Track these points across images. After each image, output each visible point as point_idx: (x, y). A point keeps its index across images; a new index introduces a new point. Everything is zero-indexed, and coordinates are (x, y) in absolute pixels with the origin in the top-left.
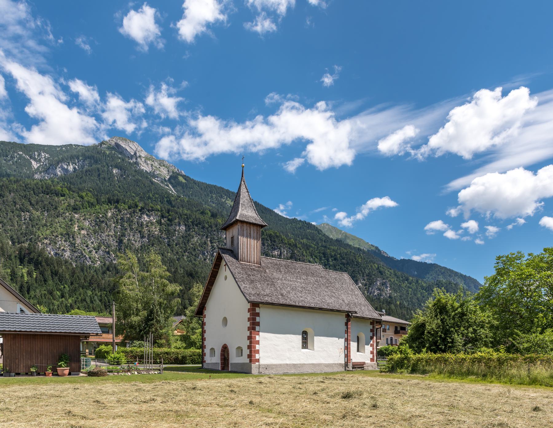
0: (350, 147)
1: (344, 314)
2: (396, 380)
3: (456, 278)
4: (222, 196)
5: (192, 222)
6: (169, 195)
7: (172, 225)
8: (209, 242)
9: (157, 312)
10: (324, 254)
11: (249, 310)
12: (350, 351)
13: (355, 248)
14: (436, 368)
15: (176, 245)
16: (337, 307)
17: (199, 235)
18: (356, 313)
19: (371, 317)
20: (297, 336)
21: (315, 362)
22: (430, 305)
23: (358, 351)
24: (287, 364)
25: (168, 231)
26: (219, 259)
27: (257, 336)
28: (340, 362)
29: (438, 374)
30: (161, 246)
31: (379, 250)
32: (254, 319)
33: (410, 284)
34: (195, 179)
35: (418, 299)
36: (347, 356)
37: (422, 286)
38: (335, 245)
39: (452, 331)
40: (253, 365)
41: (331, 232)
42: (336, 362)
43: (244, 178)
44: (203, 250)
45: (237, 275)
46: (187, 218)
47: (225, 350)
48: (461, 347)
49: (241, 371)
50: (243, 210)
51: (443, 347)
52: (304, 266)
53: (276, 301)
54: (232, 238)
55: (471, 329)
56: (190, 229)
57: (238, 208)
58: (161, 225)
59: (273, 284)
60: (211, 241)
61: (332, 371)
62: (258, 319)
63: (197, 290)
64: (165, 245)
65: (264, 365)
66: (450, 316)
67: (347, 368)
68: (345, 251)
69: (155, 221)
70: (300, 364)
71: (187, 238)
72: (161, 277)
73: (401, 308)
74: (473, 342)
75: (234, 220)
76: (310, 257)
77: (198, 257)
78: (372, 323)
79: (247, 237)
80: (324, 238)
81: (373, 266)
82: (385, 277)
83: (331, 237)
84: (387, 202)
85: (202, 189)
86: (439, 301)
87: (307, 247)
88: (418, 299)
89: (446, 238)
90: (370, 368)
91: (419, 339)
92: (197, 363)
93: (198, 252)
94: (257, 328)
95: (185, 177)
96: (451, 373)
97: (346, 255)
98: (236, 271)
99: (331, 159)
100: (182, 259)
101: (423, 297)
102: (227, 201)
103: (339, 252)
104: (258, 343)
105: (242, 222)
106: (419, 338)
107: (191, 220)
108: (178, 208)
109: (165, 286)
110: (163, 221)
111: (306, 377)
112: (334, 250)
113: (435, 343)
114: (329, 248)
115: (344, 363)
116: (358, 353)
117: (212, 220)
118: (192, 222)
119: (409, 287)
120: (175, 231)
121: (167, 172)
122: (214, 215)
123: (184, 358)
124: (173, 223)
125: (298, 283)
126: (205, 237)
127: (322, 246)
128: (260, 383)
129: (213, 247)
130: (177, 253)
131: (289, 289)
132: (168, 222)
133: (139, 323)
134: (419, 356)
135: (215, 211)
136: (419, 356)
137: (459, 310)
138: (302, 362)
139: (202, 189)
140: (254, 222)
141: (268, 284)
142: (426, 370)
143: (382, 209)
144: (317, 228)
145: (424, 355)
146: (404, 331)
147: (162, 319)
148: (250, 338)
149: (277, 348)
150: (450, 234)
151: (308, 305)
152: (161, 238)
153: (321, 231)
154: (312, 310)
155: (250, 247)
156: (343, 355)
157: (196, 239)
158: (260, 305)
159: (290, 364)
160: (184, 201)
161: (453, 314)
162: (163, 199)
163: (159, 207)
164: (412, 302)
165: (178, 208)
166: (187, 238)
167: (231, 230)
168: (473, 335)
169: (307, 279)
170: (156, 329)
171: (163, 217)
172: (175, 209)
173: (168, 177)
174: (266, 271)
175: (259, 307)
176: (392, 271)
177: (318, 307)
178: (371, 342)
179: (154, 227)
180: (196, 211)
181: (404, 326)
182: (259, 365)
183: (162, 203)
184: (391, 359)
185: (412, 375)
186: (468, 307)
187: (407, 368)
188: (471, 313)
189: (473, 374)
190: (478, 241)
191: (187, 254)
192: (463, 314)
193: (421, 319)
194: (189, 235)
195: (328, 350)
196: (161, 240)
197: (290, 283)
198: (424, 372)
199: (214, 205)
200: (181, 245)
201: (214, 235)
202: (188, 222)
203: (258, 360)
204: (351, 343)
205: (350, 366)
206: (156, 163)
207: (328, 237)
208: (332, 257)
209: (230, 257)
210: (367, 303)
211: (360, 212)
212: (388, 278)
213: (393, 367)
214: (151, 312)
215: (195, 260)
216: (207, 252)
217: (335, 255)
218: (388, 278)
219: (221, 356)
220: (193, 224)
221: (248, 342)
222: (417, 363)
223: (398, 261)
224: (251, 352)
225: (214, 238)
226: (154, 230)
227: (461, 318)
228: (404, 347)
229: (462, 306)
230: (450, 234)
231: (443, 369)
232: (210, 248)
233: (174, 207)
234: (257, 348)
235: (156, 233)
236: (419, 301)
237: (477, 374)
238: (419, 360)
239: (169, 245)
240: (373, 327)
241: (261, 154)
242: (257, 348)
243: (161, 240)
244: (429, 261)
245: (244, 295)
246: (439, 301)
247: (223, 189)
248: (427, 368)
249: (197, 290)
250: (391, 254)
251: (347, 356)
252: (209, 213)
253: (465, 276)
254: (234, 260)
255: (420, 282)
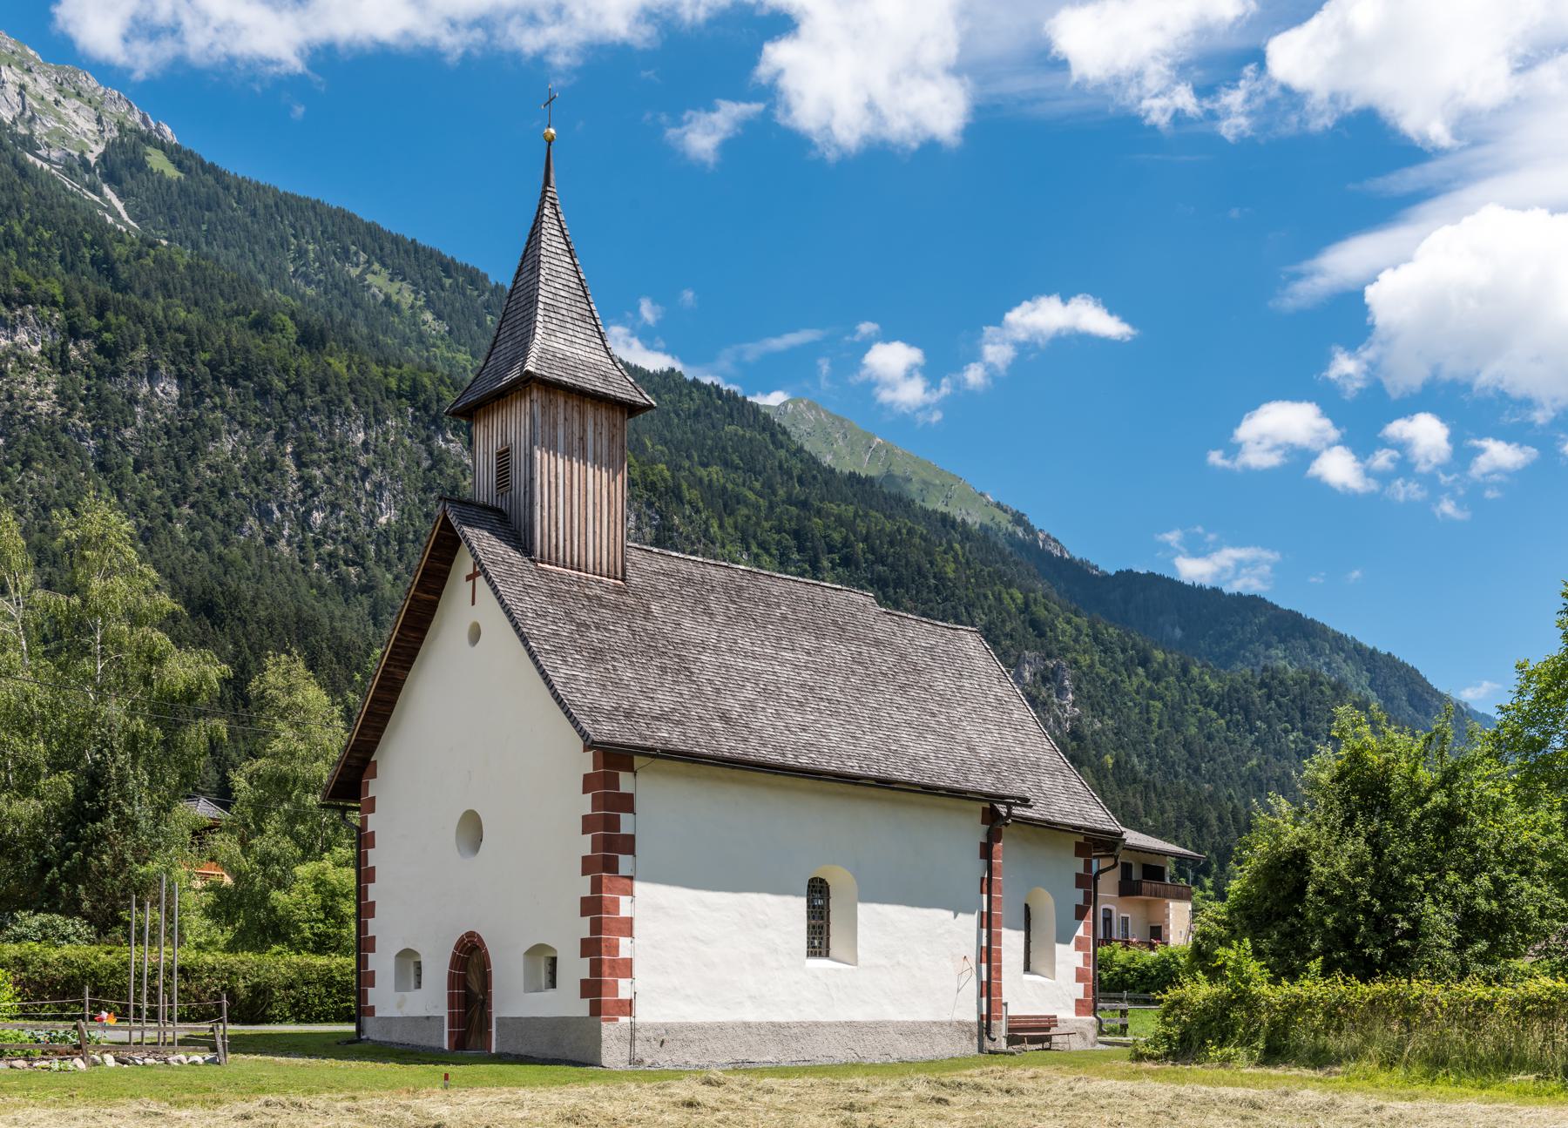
0: (956, 70)
1: (978, 807)
2: (1240, 1093)
3: (1339, 658)
4: (346, 251)
5: (213, 366)
6: (102, 235)
7: (116, 373)
8: (289, 462)
9: (122, 781)
10: (797, 534)
11: (588, 783)
12: (999, 970)
13: (928, 515)
14: (1368, 1040)
15: (137, 470)
16: (948, 777)
17: (243, 425)
18: (1025, 802)
19: (1079, 822)
20: (790, 899)
21: (859, 1015)
22: (1324, 777)
23: (1027, 969)
24: (747, 1025)
25: (101, 399)
26: (446, 546)
27: (624, 901)
28: (960, 1016)
29: (1381, 1064)
30: (64, 468)
31: (1029, 529)
32: (613, 824)
33: (1157, 680)
34: (222, 164)
35: (1187, 745)
36: (989, 989)
37: (1204, 692)
38: (845, 500)
39: (1412, 887)
40: (607, 1029)
41: (828, 440)
42: (946, 1018)
43: (553, 191)
44: (264, 495)
45: (530, 625)
46: (188, 344)
47: (470, 958)
48: (1446, 954)
49: (551, 1054)
50: (550, 333)
51: (1380, 952)
52: (801, 590)
53: (703, 746)
54: (504, 455)
55: (1483, 881)
56: (201, 397)
57: (530, 321)
58: (64, 372)
59: (684, 669)
60: (297, 456)
61: (928, 1056)
62: (626, 824)
63: (281, 682)
64: (84, 468)
65: (654, 1027)
66: (1402, 826)
67: (988, 1044)
68: (888, 526)
69: (36, 349)
70: (800, 1024)
71: (186, 436)
72: (136, 619)
73: (1120, 784)
74: (1491, 932)
75: (515, 374)
76: (738, 546)
77: (238, 530)
78: (1081, 850)
79: (569, 454)
80: (797, 467)
81: (1006, 599)
82: (1054, 648)
83: (828, 460)
84: (1094, 319)
85: (254, 214)
86: (1356, 757)
87: (726, 503)
88: (1187, 745)
89: (1321, 488)
90: (1076, 1044)
91: (1283, 917)
92: (317, 1019)
93: (237, 503)
94: (625, 862)
95: (176, 155)
96: (1436, 1063)
97: (892, 543)
98: (524, 606)
99: (871, 107)
100: (163, 535)
101: (1210, 738)
102: (370, 278)
103: (862, 528)
104: (627, 927)
105: (551, 387)
106: (1281, 914)
107: (206, 356)
108: (146, 295)
109: (154, 659)
110: (74, 353)
111: (861, 1082)
112: (840, 520)
113: (1345, 936)
114: (819, 512)
115: (974, 1018)
116: (1028, 977)
117: (305, 361)
118: (213, 366)
119: (1152, 695)
120: (133, 400)
121: (94, 127)
122: (311, 339)
123: (260, 992)
124: (120, 364)
125: (785, 665)
126: (269, 438)
127: (790, 500)
128: (690, 1105)
129: (306, 482)
130: (142, 505)
131: (749, 693)
132: (100, 360)
133: (34, 827)
134: (1296, 990)
135: (317, 318)
136: (1296, 990)
137: (1439, 798)
138: (810, 1014)
139: (254, 214)
140: (600, 387)
141: (663, 669)
142: (1325, 1050)
143: (1074, 343)
144: (767, 417)
145: (1312, 987)
146: (1155, 885)
147: (142, 812)
148: (592, 906)
149: (706, 954)
150: (1338, 468)
151: (833, 766)
152: (65, 429)
153: (785, 432)
154: (850, 788)
155: (579, 497)
156: (972, 987)
157: (228, 444)
158: (638, 761)
159: (759, 1025)
160: (173, 266)
161: (1415, 813)
162: (76, 248)
163: (56, 290)
164: (1164, 760)
165: (146, 295)
166: (186, 436)
167: (496, 421)
168: (1495, 904)
169: (818, 650)
170: (120, 862)
171: (73, 332)
172: (134, 298)
173: (99, 149)
174: (649, 612)
175: (630, 768)
176: (1082, 622)
177: (874, 773)
178: (1080, 932)
179: (30, 379)
180: (228, 316)
181: (1156, 861)
182: (633, 1029)
183: (70, 268)
184: (1178, 1003)
185: (1273, 1072)
186: (1471, 786)
187: (1247, 1042)
188: (1482, 813)
189: (1522, 1065)
190: (1448, 507)
191: (186, 510)
192: (1450, 818)
193: (1292, 835)
194: (198, 423)
195: (913, 963)
196: (64, 439)
197: (753, 665)
198: (1320, 1059)
199: (310, 292)
200: (161, 470)
201: (314, 427)
202: (193, 363)
203: (627, 1007)
204: (1004, 931)
205: (1000, 1029)
206: (43, 81)
207: (813, 461)
208: (831, 549)
209: (494, 541)
210: (1059, 760)
211: (976, 356)
212: (1065, 650)
213: (1185, 1038)
214: (95, 779)
215: (225, 541)
216: (281, 508)
217: (846, 543)
218: (1065, 650)
219: (451, 986)
220: (217, 373)
221: (584, 927)
222: (1288, 1020)
223: (1106, 577)
224: (596, 968)
225: (311, 445)
226: (34, 393)
227: (1445, 832)
228: (1232, 954)
229: (1448, 779)
230: (1338, 468)
231: (1400, 1047)
232: (292, 488)
233: (125, 289)
234: (624, 953)
235: (43, 407)
236: (1191, 753)
237: (1539, 1067)
238: (1295, 1008)
239: (102, 467)
240: (1088, 866)
241: (560, 60)
242: (624, 953)
243: (64, 439)
244: (1233, 587)
245: (569, 715)
246: (1356, 757)
247: (351, 218)
248: (1333, 1043)
249: (281, 682)
250: (1076, 550)
251: (989, 989)
252: (290, 324)
253: (1373, 652)
254: (515, 556)
255: (1195, 671)
